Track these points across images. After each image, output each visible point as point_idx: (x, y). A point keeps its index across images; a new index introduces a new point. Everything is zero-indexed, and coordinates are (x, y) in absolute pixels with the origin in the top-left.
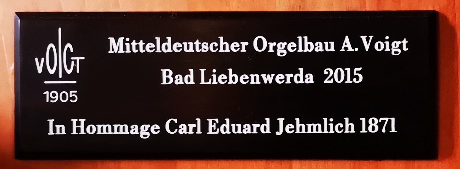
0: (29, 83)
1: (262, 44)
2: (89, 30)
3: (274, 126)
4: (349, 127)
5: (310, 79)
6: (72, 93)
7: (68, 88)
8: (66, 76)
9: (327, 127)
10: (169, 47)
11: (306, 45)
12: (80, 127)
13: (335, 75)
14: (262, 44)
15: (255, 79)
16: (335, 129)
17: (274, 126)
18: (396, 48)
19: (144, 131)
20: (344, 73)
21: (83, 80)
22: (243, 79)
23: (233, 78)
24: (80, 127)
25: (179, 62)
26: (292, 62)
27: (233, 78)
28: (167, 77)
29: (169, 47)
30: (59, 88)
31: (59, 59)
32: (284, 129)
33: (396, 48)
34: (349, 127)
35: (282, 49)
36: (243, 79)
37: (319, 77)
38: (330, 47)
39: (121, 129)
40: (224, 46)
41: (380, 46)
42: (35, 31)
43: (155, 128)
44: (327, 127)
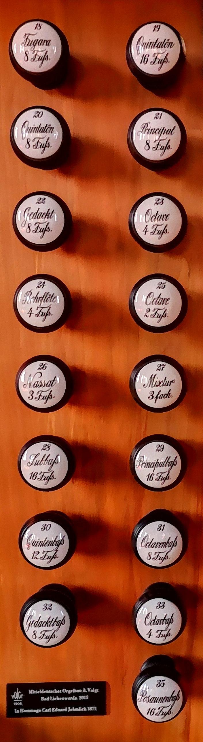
0: (10, 701)
1: (65, 691)
2: (24, 688)
3: (68, 710)
4: (85, 709)
5: (76, 699)
6: (21, 703)
7: (20, 702)
8: (19, 699)
9: (80, 709)
10: (43, 692)
11: (75, 691)
12: (22, 711)
13: (82, 698)
14: (65, 691)
15: (63, 699)
16: (82, 710)
17: (68, 710)
18: (96, 691)
19: (38, 711)
20: (133, 40)
21: (23, 700)
22: (60, 699)
23: (58, 699)
24: (22, 711)
25: (46, 695)
26: (72, 695)
27: (58, 699)
28: (43, 699)
29: (43, 692)
30: (17, 702)
31: (17, 695)
32: (70, 710)
33: (96, 691)
34: (84, 690)
35: (70, 692)
36: (60, 699)
37: (78, 698)
38: (80, 691)
39: (32, 711)
40: (56, 691)
41: (92, 691)
42: (11, 688)
43: (40, 711)
44: (80, 709)
